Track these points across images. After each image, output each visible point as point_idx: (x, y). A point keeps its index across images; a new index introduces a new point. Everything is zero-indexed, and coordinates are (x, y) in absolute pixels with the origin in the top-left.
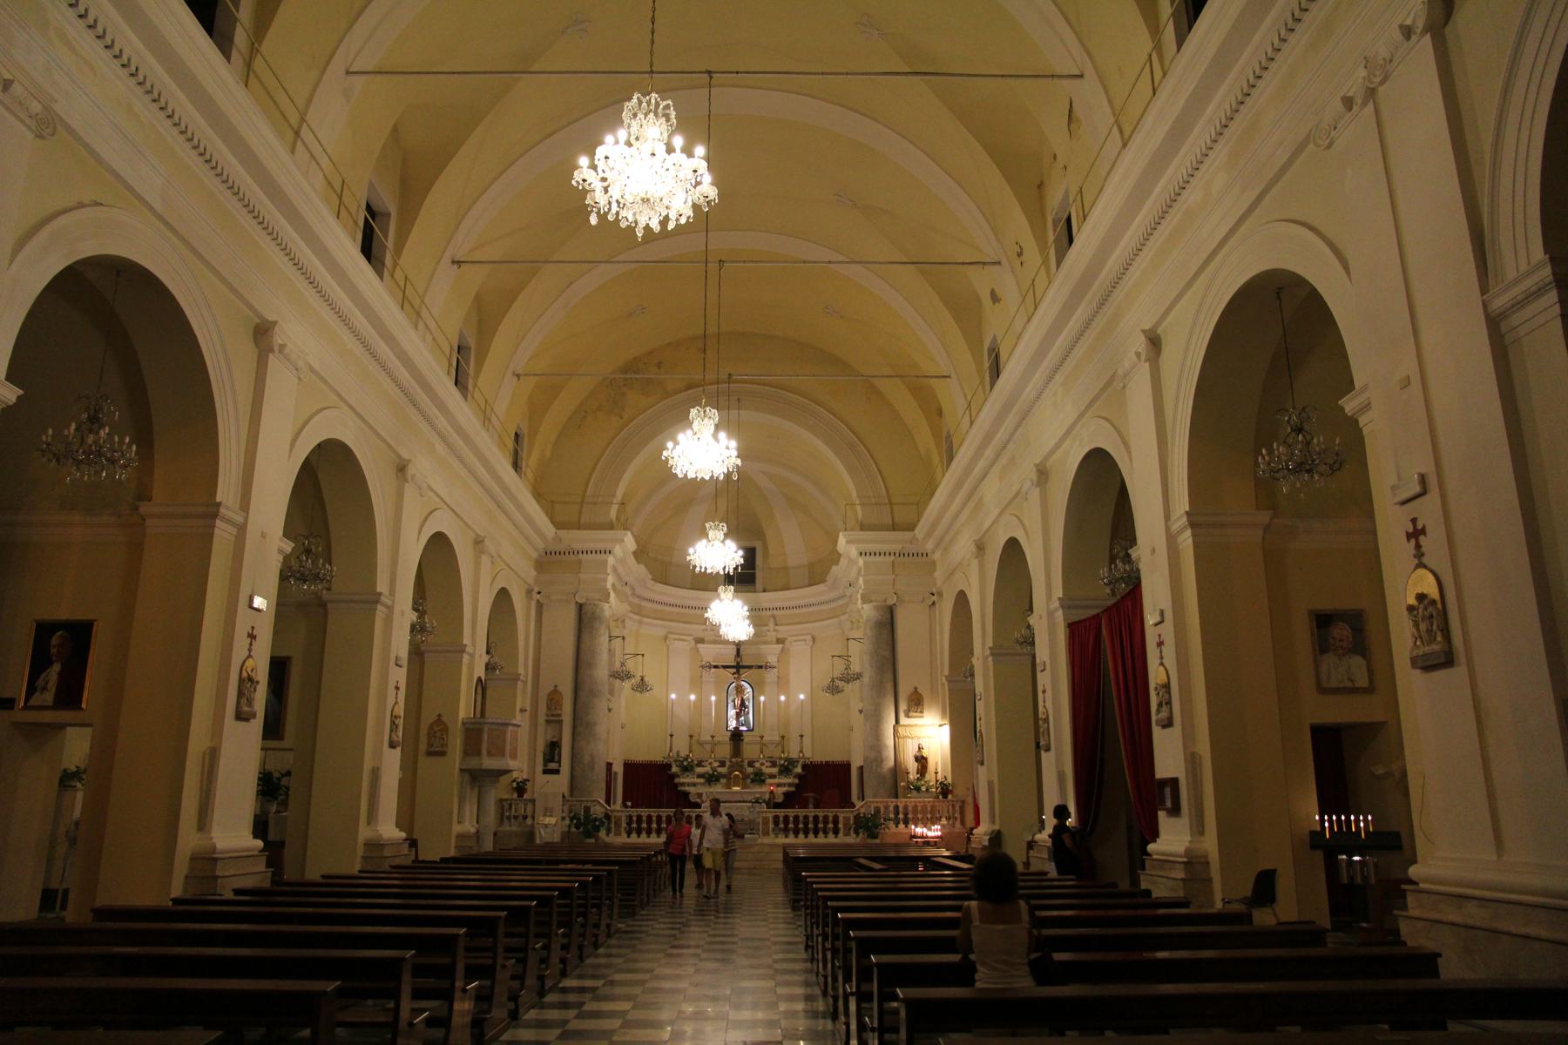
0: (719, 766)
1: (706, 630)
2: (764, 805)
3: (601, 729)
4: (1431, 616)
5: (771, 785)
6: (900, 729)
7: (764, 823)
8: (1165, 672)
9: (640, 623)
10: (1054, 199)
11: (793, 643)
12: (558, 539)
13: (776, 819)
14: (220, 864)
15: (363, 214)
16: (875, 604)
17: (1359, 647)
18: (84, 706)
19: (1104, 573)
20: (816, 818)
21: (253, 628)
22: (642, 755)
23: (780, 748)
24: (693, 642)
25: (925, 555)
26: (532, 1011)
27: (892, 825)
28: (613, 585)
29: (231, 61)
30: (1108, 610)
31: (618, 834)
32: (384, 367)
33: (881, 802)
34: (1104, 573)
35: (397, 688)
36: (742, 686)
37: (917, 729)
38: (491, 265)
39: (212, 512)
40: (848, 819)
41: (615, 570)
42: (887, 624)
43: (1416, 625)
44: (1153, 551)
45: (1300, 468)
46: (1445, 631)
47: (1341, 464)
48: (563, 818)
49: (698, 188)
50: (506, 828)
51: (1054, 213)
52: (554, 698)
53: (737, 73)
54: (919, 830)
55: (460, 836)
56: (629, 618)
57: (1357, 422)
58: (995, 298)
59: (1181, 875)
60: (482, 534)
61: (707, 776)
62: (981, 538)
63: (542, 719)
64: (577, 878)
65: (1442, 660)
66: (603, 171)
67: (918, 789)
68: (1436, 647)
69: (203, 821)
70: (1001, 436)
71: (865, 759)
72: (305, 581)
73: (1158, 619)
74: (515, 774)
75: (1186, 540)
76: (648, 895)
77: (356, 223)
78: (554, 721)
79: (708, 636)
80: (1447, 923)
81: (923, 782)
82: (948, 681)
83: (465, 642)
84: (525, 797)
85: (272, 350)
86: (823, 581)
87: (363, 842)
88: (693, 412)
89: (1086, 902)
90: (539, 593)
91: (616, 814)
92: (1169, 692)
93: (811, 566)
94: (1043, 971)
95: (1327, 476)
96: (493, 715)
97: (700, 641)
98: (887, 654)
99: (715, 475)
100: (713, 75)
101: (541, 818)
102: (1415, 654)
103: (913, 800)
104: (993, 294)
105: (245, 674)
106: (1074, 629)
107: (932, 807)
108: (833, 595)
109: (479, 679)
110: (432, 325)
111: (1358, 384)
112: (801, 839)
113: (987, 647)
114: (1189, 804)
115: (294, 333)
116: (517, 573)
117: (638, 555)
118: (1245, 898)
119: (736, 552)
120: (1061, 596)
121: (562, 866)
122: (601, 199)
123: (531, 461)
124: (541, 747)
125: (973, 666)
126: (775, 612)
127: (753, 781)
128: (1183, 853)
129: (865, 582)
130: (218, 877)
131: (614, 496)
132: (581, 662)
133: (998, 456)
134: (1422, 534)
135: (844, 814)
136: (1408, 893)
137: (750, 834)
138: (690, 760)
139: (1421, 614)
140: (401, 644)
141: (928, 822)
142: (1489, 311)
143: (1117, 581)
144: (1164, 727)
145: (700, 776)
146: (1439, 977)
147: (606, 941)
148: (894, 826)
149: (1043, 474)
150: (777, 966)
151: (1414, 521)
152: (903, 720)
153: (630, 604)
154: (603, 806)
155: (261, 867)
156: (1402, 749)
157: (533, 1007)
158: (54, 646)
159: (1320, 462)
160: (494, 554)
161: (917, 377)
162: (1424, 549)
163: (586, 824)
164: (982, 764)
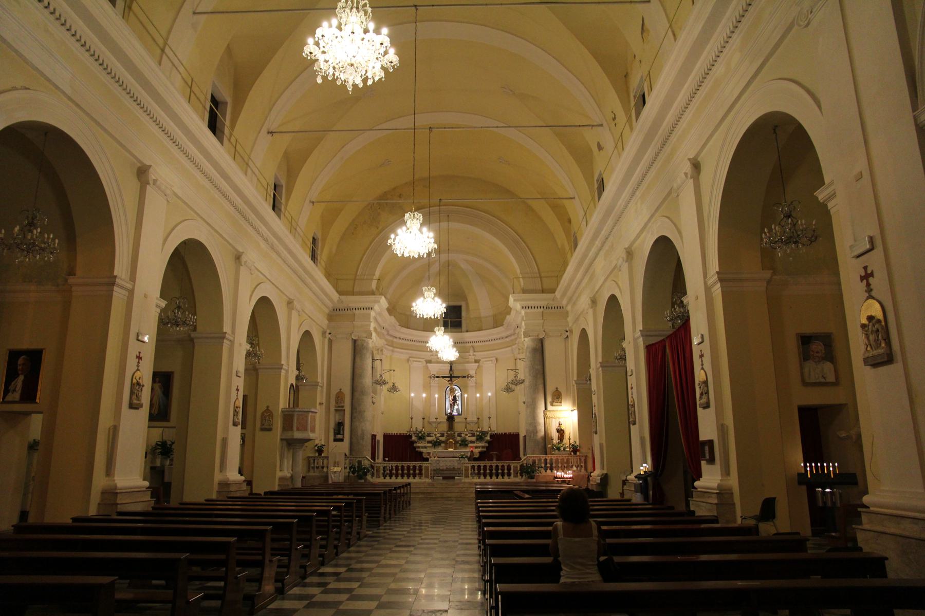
0: (440, 436)
1: (432, 355)
2: (466, 459)
3: (368, 414)
4: (878, 330)
5: (472, 447)
6: (548, 413)
7: (465, 470)
8: (704, 373)
9: (393, 351)
10: (634, 83)
11: (485, 363)
12: (340, 301)
13: (473, 467)
14: (119, 496)
15: (208, 104)
16: (532, 337)
17: (829, 356)
18: (37, 401)
19: (667, 314)
20: (497, 466)
21: (140, 353)
22: (394, 431)
23: (477, 425)
24: (425, 363)
25: (562, 308)
26: (295, 588)
27: (543, 470)
28: (375, 329)
29: (117, 6)
30: (669, 337)
31: (378, 477)
32: (224, 195)
33: (536, 457)
34: (667, 314)
35: (238, 390)
36: (453, 388)
37: (558, 413)
38: (293, 134)
39: (111, 282)
40: (517, 467)
41: (375, 319)
42: (539, 350)
43: (867, 337)
44: (697, 298)
45: (788, 241)
46: (887, 340)
47: (816, 238)
48: (345, 468)
49: (386, 56)
50: (312, 474)
51: (634, 91)
52: (340, 396)
53: (433, 6)
54: (559, 474)
55: (281, 479)
56: (385, 348)
57: (827, 205)
58: (600, 148)
59: (716, 501)
60: (292, 297)
61: (433, 442)
62: (594, 296)
63: (332, 409)
64: (344, 501)
65: (886, 359)
66: (324, 47)
67: (558, 449)
68: (881, 351)
69: (109, 470)
70: (603, 233)
71: (527, 431)
72: (177, 325)
73: (700, 340)
74: (317, 442)
75: (717, 290)
76: (390, 514)
77: (204, 107)
78: (340, 410)
79: (433, 359)
80: (889, 534)
81: (562, 445)
82: (576, 384)
83: (282, 363)
84: (323, 455)
85: (149, 183)
86: (502, 325)
87: (217, 483)
88: (407, 215)
89: (658, 519)
90: (330, 334)
91: (377, 465)
92: (707, 386)
93: (494, 316)
94: (608, 572)
95: (808, 245)
96: (302, 406)
97: (429, 362)
98: (539, 367)
99: (421, 255)
100: (417, 8)
101: (332, 468)
102: (867, 355)
103: (555, 456)
104: (599, 144)
105: (135, 381)
106: (649, 349)
107: (567, 460)
108: (509, 333)
109: (292, 385)
110: (257, 172)
111: (827, 180)
112: (488, 479)
113: (598, 362)
114: (720, 457)
115: (162, 172)
116: (317, 323)
117: (391, 310)
118: (756, 516)
119: (441, 305)
120: (641, 329)
121: (335, 497)
122: (323, 66)
123: (323, 256)
124: (332, 425)
125: (590, 374)
126: (474, 344)
127: (460, 445)
128: (716, 487)
129: (525, 325)
130: (118, 504)
131: (374, 275)
132: (355, 375)
133: (603, 244)
134: (871, 276)
135: (514, 464)
136: (862, 513)
137: (437, 476)
138: (423, 433)
139: (870, 330)
140: (240, 363)
141: (565, 468)
142: (918, 123)
143: (676, 318)
144: (704, 408)
145: (429, 442)
146: (886, 577)
147: (356, 543)
148: (544, 471)
149: (630, 254)
150: (459, 559)
151: (865, 268)
152: (550, 407)
153: (386, 340)
154: (369, 460)
155: (147, 497)
156: (857, 419)
157: (296, 586)
158: (20, 365)
159: (803, 236)
160: (301, 310)
161: (554, 198)
162: (872, 287)
163: (358, 471)
164: (596, 433)
